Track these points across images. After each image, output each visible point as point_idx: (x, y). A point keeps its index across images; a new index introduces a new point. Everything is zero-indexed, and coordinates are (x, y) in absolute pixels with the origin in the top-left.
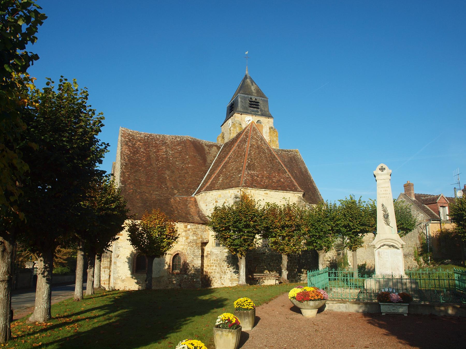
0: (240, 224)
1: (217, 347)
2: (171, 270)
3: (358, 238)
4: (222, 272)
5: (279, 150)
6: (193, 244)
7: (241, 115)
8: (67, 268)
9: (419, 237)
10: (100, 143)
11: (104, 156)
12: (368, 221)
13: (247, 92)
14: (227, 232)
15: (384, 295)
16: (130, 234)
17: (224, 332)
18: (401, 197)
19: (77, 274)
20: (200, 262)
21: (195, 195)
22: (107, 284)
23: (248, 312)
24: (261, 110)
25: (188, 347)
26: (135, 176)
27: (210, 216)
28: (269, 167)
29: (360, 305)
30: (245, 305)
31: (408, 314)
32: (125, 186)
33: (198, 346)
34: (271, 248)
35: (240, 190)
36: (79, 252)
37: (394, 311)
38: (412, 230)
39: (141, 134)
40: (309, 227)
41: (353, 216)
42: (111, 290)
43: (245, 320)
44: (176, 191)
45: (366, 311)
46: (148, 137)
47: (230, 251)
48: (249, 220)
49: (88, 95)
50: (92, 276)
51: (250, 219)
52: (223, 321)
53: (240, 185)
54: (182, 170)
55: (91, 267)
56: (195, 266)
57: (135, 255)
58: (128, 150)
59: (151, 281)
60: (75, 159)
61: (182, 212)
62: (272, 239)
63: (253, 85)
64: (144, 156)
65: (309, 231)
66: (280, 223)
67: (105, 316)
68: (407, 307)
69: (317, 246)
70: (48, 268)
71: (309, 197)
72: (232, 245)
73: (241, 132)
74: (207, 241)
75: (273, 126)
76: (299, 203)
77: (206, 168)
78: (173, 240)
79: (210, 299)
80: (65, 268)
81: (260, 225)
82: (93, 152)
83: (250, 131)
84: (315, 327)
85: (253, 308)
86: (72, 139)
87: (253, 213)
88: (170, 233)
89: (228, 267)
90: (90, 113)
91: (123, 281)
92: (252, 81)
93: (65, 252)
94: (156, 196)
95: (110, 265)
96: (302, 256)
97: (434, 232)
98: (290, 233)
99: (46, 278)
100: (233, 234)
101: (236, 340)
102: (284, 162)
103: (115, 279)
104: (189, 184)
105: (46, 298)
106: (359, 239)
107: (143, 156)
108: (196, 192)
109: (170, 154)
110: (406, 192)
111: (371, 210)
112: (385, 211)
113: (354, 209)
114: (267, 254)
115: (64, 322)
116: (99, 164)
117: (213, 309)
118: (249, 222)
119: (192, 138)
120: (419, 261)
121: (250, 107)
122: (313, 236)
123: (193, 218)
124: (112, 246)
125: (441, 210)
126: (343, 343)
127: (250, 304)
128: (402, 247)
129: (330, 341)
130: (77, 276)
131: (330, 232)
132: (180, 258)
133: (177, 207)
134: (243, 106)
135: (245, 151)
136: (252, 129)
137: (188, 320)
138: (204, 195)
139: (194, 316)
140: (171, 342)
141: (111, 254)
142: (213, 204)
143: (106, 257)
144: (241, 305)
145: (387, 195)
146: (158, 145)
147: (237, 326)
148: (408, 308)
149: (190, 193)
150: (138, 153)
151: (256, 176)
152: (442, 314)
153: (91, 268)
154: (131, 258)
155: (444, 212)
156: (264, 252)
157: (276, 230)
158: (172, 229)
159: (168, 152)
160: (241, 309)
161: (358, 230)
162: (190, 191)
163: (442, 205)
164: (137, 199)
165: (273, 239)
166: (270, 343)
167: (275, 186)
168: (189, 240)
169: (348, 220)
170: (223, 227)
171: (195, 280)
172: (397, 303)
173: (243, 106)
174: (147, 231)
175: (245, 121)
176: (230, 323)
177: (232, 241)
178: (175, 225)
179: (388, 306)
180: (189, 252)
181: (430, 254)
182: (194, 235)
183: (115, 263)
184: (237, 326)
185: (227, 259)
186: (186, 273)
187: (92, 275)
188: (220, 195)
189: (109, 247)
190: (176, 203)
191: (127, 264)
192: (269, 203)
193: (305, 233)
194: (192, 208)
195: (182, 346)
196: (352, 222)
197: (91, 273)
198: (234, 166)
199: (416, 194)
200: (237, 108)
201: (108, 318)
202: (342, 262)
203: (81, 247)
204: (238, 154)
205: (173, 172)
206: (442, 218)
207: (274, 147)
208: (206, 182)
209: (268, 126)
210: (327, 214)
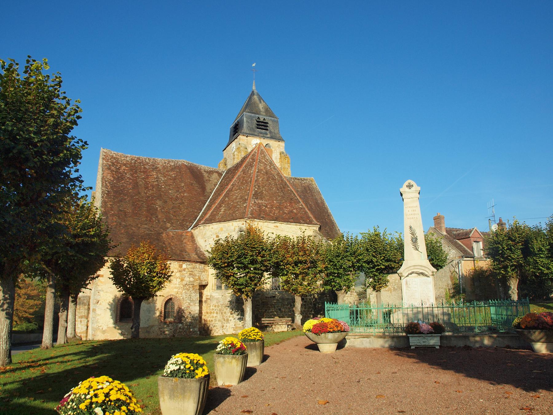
0: (245, 259)
2: (163, 318)
4: (224, 320)
5: (291, 178)
6: (189, 287)
7: (247, 137)
8: (34, 324)
9: (451, 277)
12: (394, 257)
13: (253, 111)
14: (230, 269)
16: (112, 272)
17: (227, 359)
19: (46, 316)
20: (198, 308)
21: (192, 229)
23: (256, 344)
24: (270, 132)
25: (182, 360)
29: (386, 339)
30: (252, 335)
33: (195, 359)
35: (246, 222)
36: (49, 289)
37: (425, 344)
39: (127, 157)
40: (326, 263)
41: (377, 251)
44: (169, 225)
45: (393, 345)
46: (136, 161)
48: (256, 254)
49: (61, 82)
50: (65, 321)
52: (225, 346)
55: (63, 310)
56: (192, 313)
57: (119, 300)
58: (110, 176)
60: (44, 154)
61: (176, 249)
62: (283, 277)
63: (261, 102)
64: (130, 183)
65: (326, 268)
66: (292, 259)
67: (80, 361)
68: (438, 339)
70: (8, 299)
71: (326, 233)
72: (236, 284)
73: (247, 155)
75: (284, 151)
77: (205, 198)
78: (165, 279)
80: (31, 324)
81: (269, 260)
82: (67, 149)
83: (258, 154)
86: (41, 131)
87: (261, 246)
89: (232, 314)
91: (104, 332)
93: (31, 304)
94: (145, 230)
95: (88, 313)
98: (305, 271)
99: (5, 311)
101: (241, 368)
102: (297, 191)
103: (94, 330)
104: (185, 216)
105: (5, 337)
106: (384, 277)
107: (129, 183)
109: (162, 181)
110: (437, 226)
112: (413, 234)
113: (378, 242)
115: (29, 366)
118: (256, 257)
119: (188, 163)
121: (258, 128)
122: (331, 274)
123: (189, 256)
125: (475, 245)
127: (257, 335)
128: (433, 275)
130: (46, 318)
131: (350, 269)
132: (173, 304)
133: (170, 243)
134: (249, 126)
136: (260, 151)
138: (203, 229)
143: (83, 304)
144: (247, 335)
145: (415, 216)
146: (147, 171)
148: (440, 339)
150: (122, 179)
152: (477, 345)
153: (63, 311)
154: (114, 304)
155: (478, 249)
156: (274, 295)
157: (287, 267)
158: (164, 265)
159: (159, 178)
160: (247, 341)
161: (383, 267)
162: (185, 224)
163: (475, 239)
164: (122, 234)
165: (284, 278)
167: (286, 218)
168: (184, 283)
170: (225, 263)
171: (191, 330)
172: (428, 334)
173: (249, 126)
175: (251, 145)
176: (234, 349)
179: (418, 338)
180: (185, 297)
183: (94, 310)
185: (231, 304)
188: (222, 228)
190: (169, 238)
191: (108, 311)
192: (280, 236)
193: (322, 270)
195: (176, 360)
196: (376, 257)
199: (447, 228)
200: (242, 130)
203: (51, 283)
204: (243, 181)
205: (165, 202)
206: (476, 255)
208: (205, 213)
209: (278, 151)
210: (348, 248)
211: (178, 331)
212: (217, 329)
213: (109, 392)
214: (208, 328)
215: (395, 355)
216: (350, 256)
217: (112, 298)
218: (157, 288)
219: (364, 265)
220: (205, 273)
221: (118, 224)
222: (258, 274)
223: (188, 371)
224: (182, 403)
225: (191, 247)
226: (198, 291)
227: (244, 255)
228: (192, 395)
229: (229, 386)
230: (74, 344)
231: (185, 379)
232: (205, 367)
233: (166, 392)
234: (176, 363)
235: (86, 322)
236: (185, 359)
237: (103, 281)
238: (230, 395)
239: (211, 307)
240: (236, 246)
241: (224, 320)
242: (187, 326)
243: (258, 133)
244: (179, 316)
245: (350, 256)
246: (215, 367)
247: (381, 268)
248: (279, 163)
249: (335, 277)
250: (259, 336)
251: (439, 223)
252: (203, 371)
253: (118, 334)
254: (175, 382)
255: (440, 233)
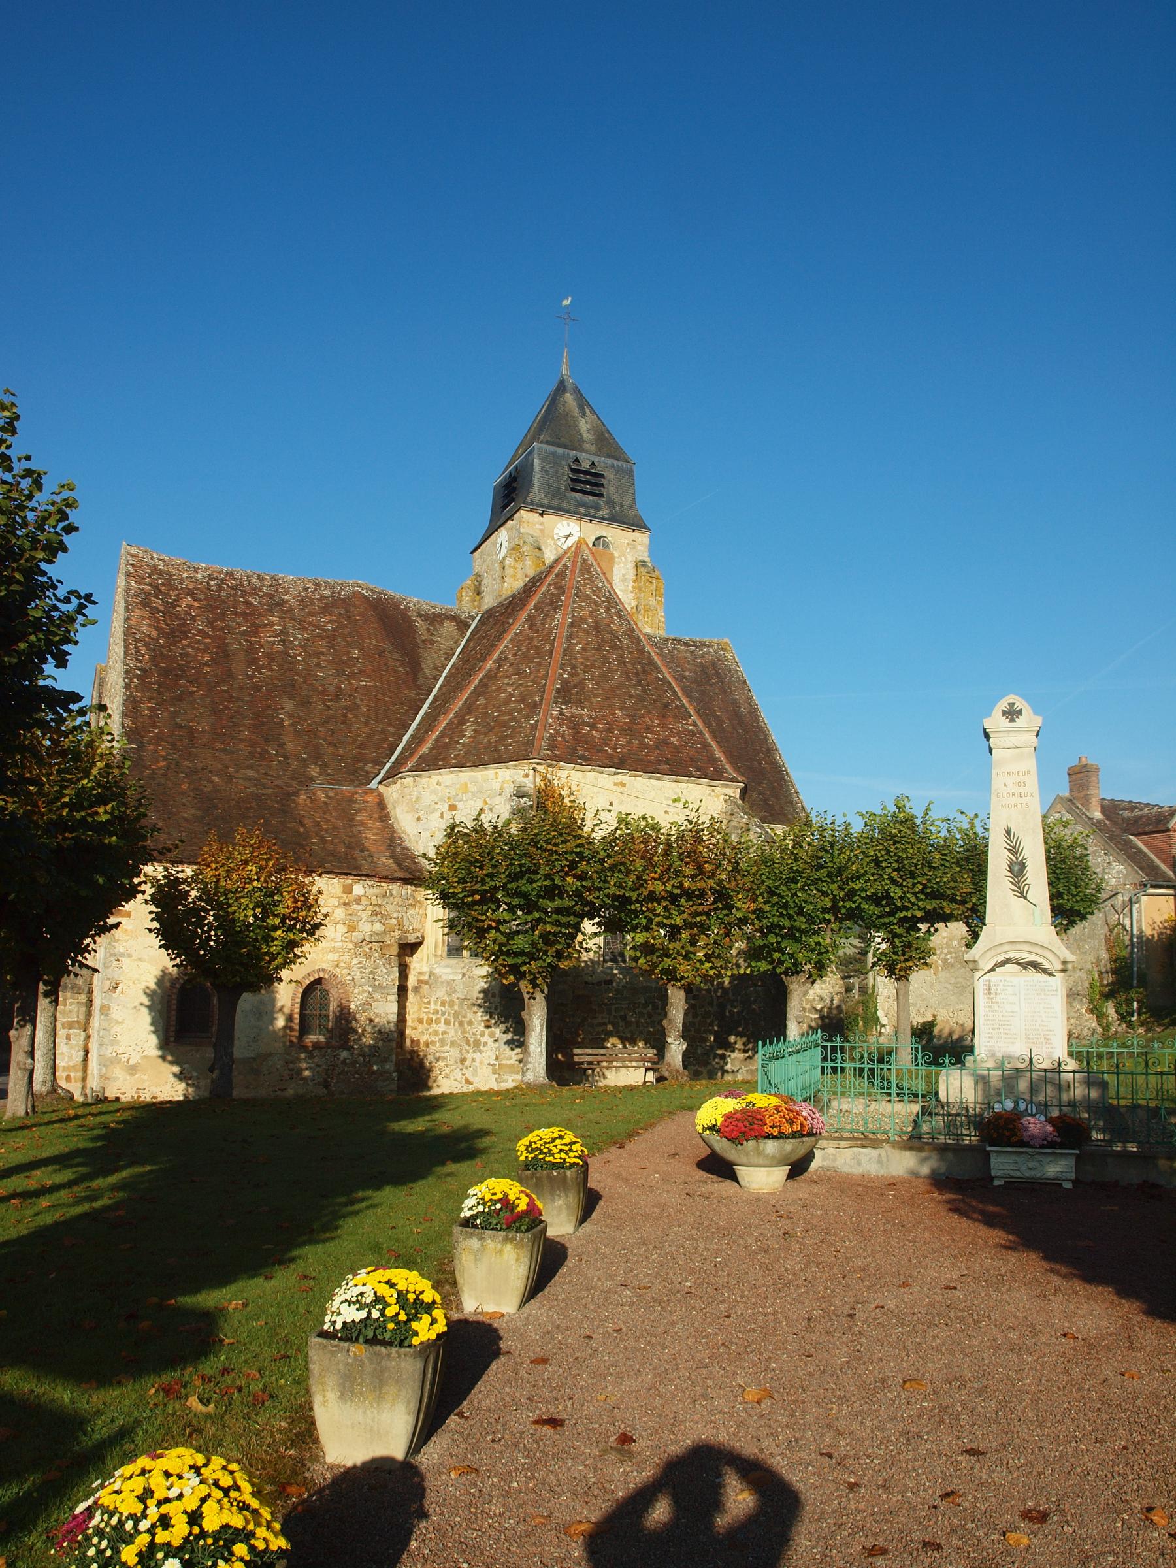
0: (531, 883)
1: (464, 1289)
2: (297, 1034)
3: (918, 938)
4: (468, 1043)
5: (666, 639)
6: (371, 949)
7: (541, 515)
9: (1107, 940)
10: (61, 592)
11: (77, 639)
12: (952, 884)
14: (487, 911)
15: (1001, 1121)
17: (489, 1241)
18: (1059, 807)
20: (394, 1008)
21: (380, 783)
22: (76, 1081)
24: (610, 503)
25: (375, 1293)
26: (176, 714)
27: (432, 854)
28: (631, 696)
29: (924, 1154)
30: (555, 1151)
31: (1073, 1182)
32: (141, 746)
33: (411, 1289)
34: (634, 964)
35: (534, 769)
37: (1032, 1173)
38: (1088, 916)
39: (196, 570)
40: (760, 899)
41: (903, 867)
42: (90, 1100)
43: (553, 1201)
44: (314, 770)
45: (943, 1170)
46: (222, 581)
47: (497, 974)
48: (562, 870)
49: (17, 417)
50: (26, 1052)
51: (567, 869)
52: (484, 1204)
53: (535, 754)
54: (336, 698)
55: (22, 1023)
56: (376, 1021)
57: (174, 981)
58: (149, 625)
59: (231, 1070)
61: (336, 841)
63: (583, 414)
65: (760, 914)
67: (75, 1189)
68: (1072, 1162)
69: (783, 962)
71: (761, 800)
72: (503, 953)
73: (541, 573)
74: (418, 937)
75: (648, 559)
76: (729, 818)
78: (305, 935)
79: (428, 1130)
81: (599, 889)
82: (37, 625)
83: (573, 571)
84: (782, 1222)
85: (581, 1163)
88: (296, 909)
89: (488, 1027)
90: (26, 483)
91: (132, 1069)
92: (582, 403)
94: (247, 784)
95: (89, 1014)
96: (731, 995)
97: (1155, 923)
98: (698, 919)
100: (507, 916)
101: (527, 1267)
102: (680, 679)
103: (105, 1063)
106: (920, 941)
107: (202, 647)
108: (383, 772)
110: (1076, 794)
111: (961, 847)
112: (1014, 851)
113: (909, 843)
114: (618, 984)
116: (57, 667)
117: (443, 1163)
119: (371, 590)
120: (1104, 1014)
121: (573, 490)
122: (772, 928)
123: (372, 862)
124: (95, 951)
126: (875, 1275)
127: (571, 1150)
128: (1064, 970)
129: (832, 1269)
131: (827, 916)
132: (325, 995)
133: (319, 822)
134: (548, 484)
135: (554, 639)
136: (579, 563)
137: (362, 1200)
138: (411, 784)
139: (378, 1188)
140: (308, 1274)
141: (92, 978)
142: (442, 817)
143: (72, 988)
144: (541, 1150)
145: (1024, 800)
147: (531, 1221)
149: (361, 775)
151: (588, 724)
153: (22, 1026)
154: (159, 991)
156: (608, 978)
157: (649, 905)
158: (303, 895)
159: (288, 634)
160: (542, 1167)
161: (919, 914)
165: (640, 937)
166: (637, 1275)
167: (650, 761)
168: (357, 936)
169: (886, 877)
171: (375, 1067)
172: (1042, 1147)
173: (548, 484)
174: (216, 901)
175: (553, 539)
176: (508, 1213)
177: (503, 939)
178: (312, 883)
180: (358, 976)
181: (1137, 992)
182: (374, 918)
183: (105, 1009)
184: (534, 1221)
185: (486, 999)
186: (345, 1046)
187: (28, 1049)
188: (466, 783)
189: (86, 954)
191: (145, 1011)
194: (369, 828)
195: (356, 1291)
197: (25, 1042)
198: (514, 690)
199: (1103, 799)
201: (87, 1193)
202: (858, 1015)
204: (529, 649)
205: (305, 703)
207: (648, 630)
208: (418, 739)
209: (630, 558)
210: (821, 858)
211: (338, 1070)
212: (447, 1066)
213: (200, 1507)
214: (422, 1063)
215: (950, 1209)
216: (826, 881)
217: (156, 977)
218: (279, 960)
219: (867, 907)
220: (417, 910)
221: (172, 766)
222: (568, 925)
223: (391, 1326)
224: (375, 1412)
225: (376, 834)
226: (395, 960)
227: (528, 871)
228: (403, 1393)
229: (493, 1315)
230: (54, 1117)
231: (383, 1349)
232: (436, 1313)
233: (331, 1381)
234: (358, 1302)
235: (82, 1039)
236: (384, 1290)
237: (130, 928)
238: (497, 1353)
239: (432, 1003)
240: (506, 844)
241: (468, 1043)
242: (364, 1056)
243: (575, 505)
244: (341, 1029)
245: (826, 881)
246: (457, 1262)
247: (914, 916)
248: (632, 592)
249: (783, 937)
250: (576, 1154)
251: (1082, 785)
252: (431, 1324)
253: (171, 1075)
254: (355, 1355)
255: (1083, 814)
